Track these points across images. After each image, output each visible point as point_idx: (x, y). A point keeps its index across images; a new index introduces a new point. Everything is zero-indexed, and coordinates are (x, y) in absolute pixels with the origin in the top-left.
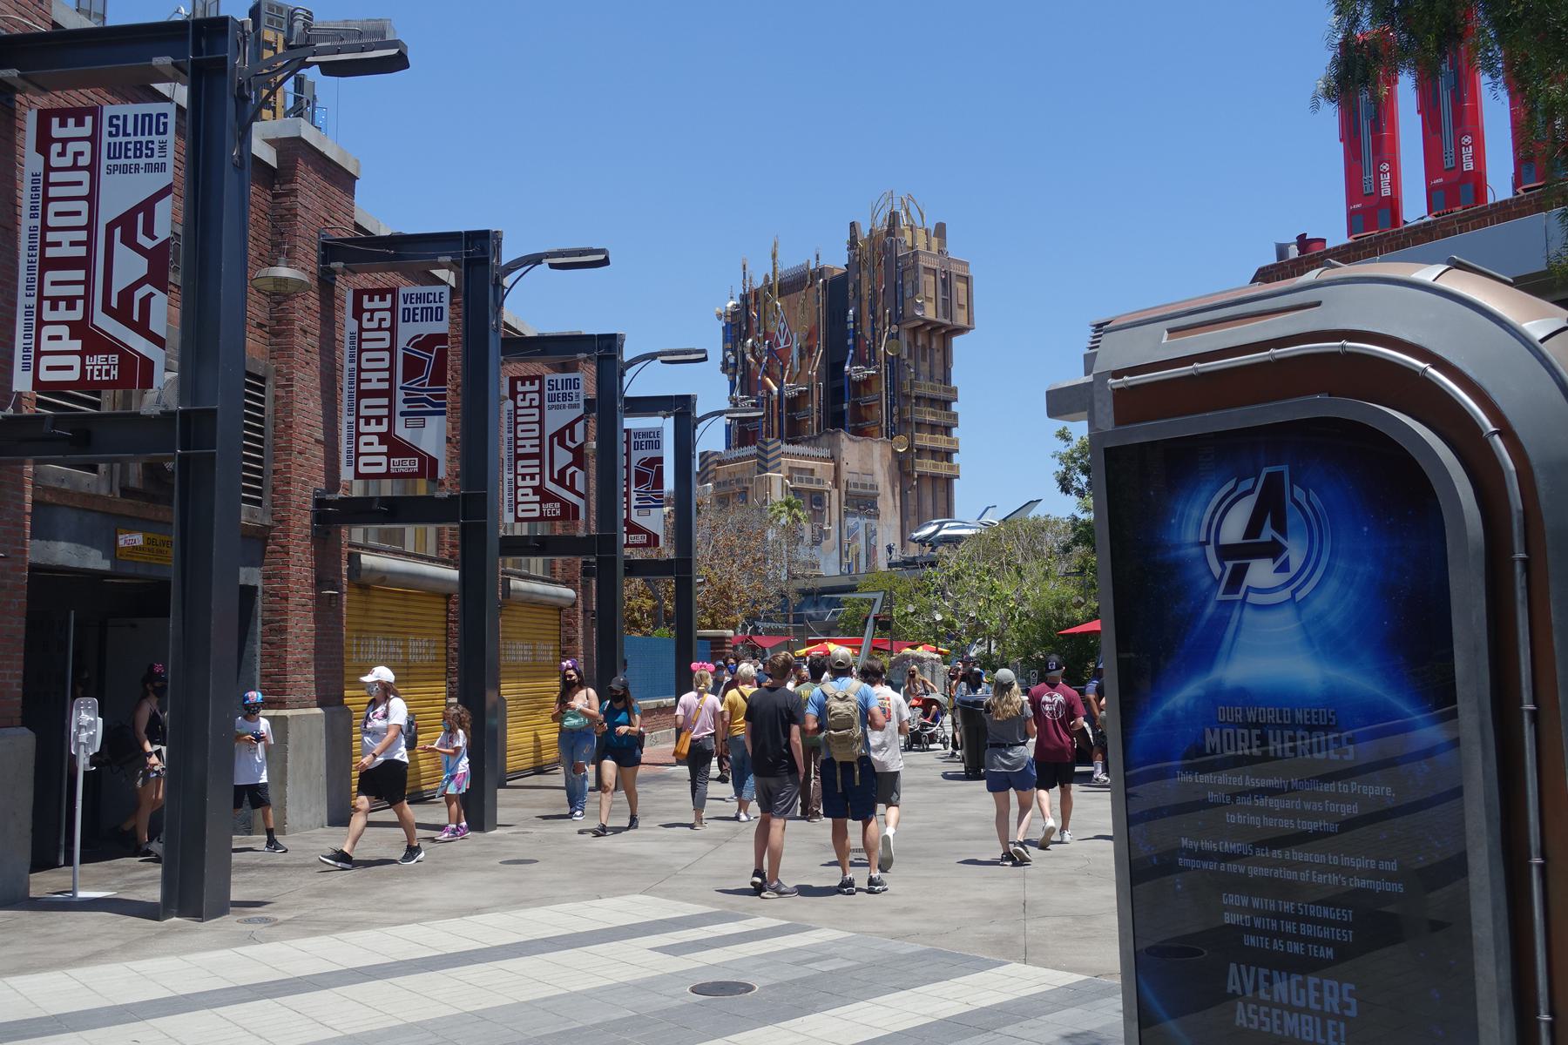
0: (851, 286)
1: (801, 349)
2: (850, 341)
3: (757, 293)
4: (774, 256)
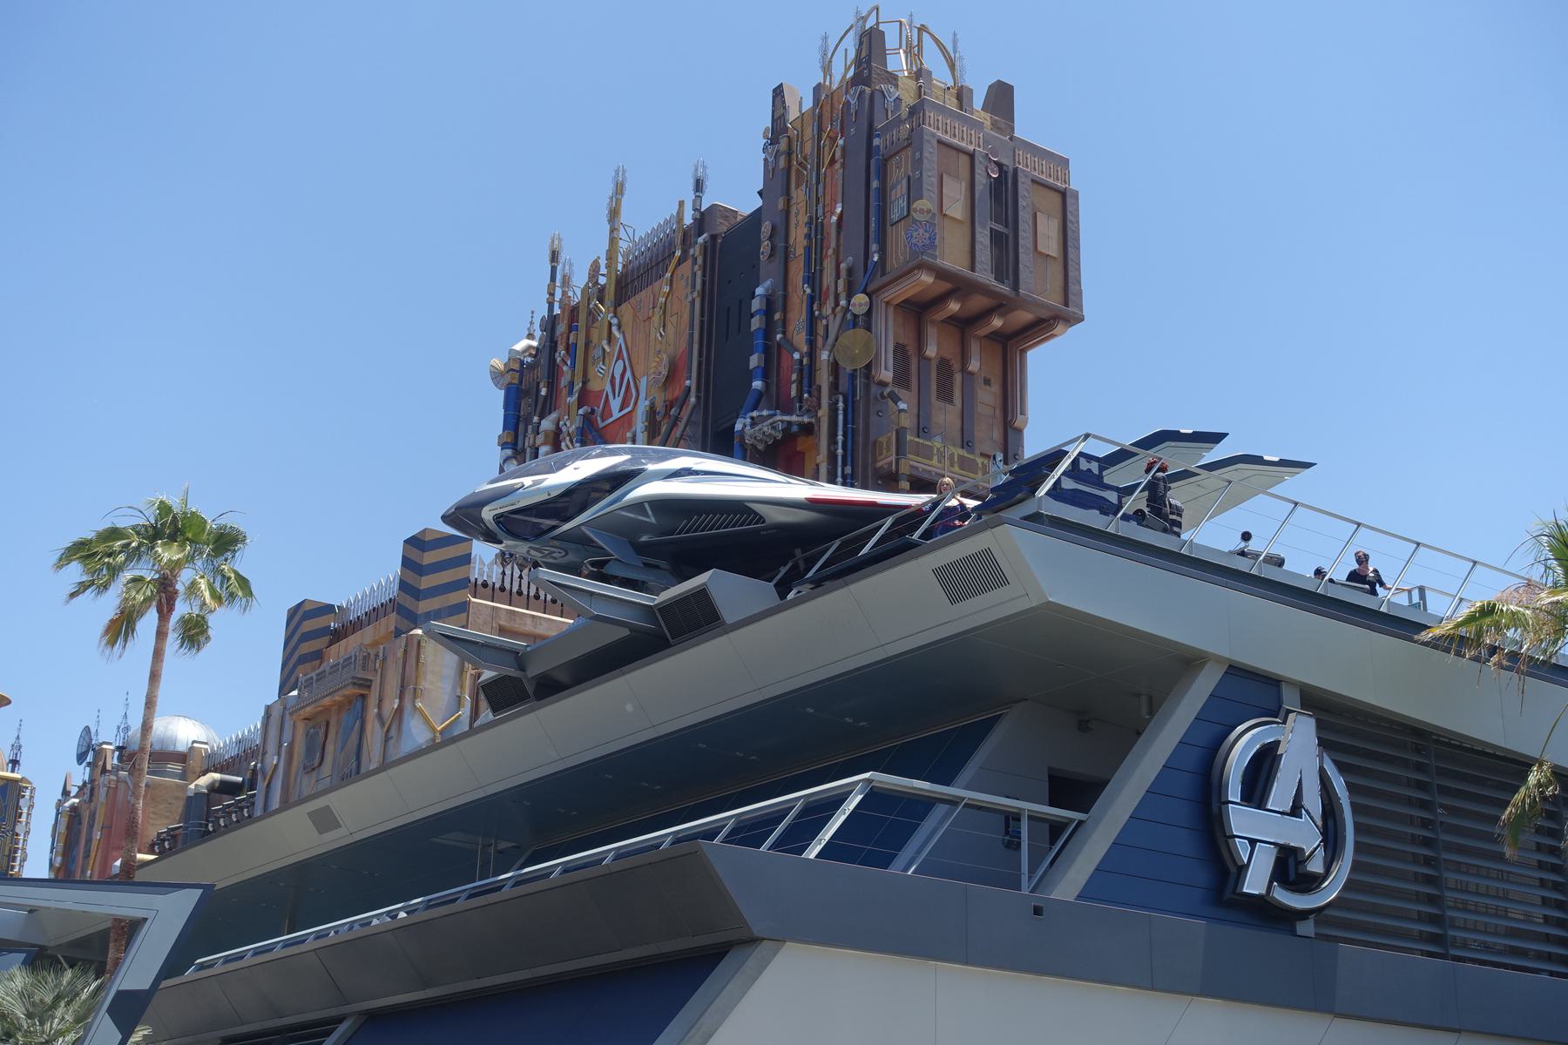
1: (652, 412)
2: (755, 361)
3: (573, 312)
4: (614, 214)
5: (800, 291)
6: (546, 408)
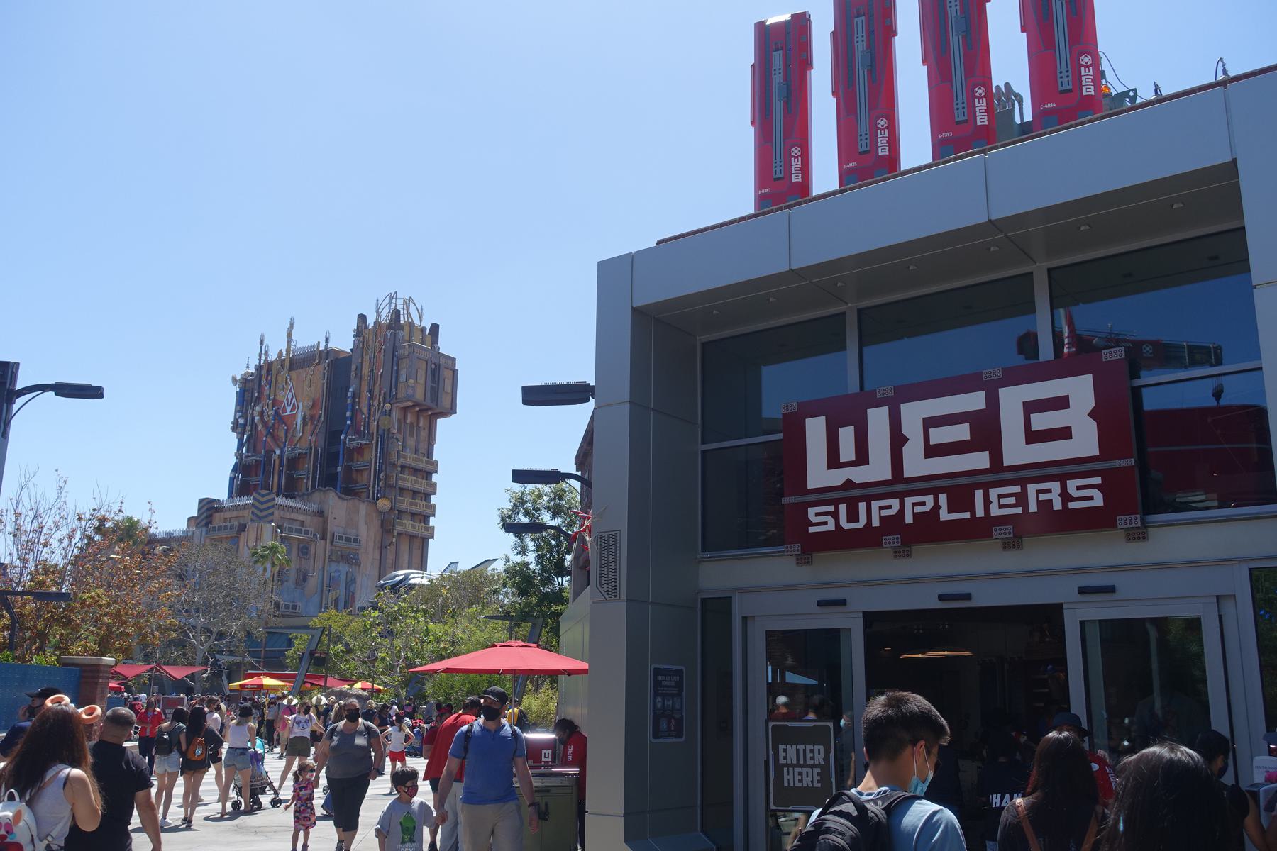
0: (354, 367)
1: (304, 418)
2: (348, 414)
4: (289, 336)
5: (365, 395)
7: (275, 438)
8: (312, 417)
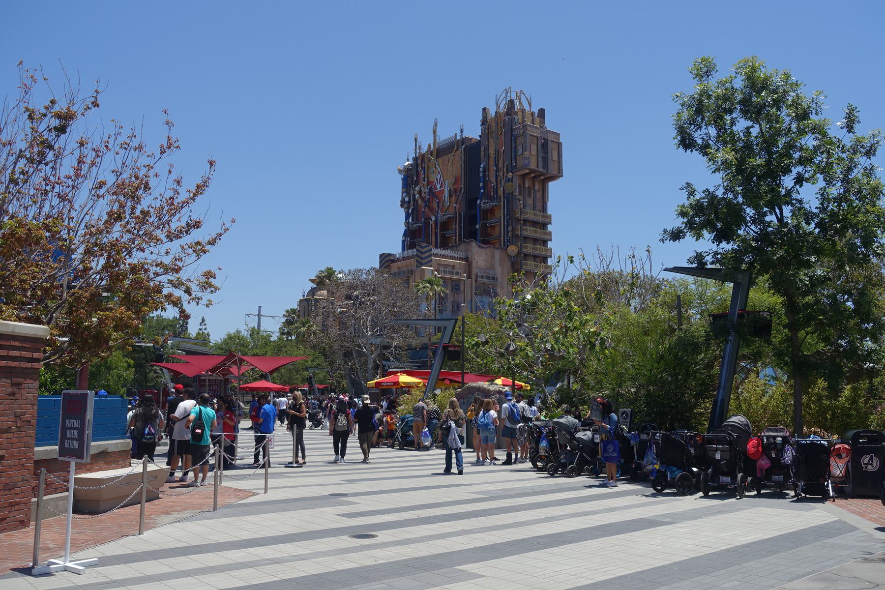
1: (450, 191)
2: (481, 185)
4: (435, 132)
5: (493, 168)
6: (416, 184)
7: (431, 209)
8: (456, 190)
